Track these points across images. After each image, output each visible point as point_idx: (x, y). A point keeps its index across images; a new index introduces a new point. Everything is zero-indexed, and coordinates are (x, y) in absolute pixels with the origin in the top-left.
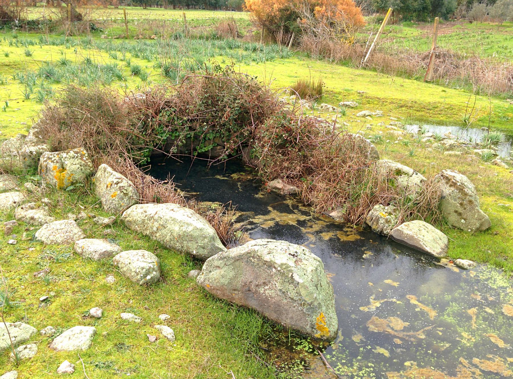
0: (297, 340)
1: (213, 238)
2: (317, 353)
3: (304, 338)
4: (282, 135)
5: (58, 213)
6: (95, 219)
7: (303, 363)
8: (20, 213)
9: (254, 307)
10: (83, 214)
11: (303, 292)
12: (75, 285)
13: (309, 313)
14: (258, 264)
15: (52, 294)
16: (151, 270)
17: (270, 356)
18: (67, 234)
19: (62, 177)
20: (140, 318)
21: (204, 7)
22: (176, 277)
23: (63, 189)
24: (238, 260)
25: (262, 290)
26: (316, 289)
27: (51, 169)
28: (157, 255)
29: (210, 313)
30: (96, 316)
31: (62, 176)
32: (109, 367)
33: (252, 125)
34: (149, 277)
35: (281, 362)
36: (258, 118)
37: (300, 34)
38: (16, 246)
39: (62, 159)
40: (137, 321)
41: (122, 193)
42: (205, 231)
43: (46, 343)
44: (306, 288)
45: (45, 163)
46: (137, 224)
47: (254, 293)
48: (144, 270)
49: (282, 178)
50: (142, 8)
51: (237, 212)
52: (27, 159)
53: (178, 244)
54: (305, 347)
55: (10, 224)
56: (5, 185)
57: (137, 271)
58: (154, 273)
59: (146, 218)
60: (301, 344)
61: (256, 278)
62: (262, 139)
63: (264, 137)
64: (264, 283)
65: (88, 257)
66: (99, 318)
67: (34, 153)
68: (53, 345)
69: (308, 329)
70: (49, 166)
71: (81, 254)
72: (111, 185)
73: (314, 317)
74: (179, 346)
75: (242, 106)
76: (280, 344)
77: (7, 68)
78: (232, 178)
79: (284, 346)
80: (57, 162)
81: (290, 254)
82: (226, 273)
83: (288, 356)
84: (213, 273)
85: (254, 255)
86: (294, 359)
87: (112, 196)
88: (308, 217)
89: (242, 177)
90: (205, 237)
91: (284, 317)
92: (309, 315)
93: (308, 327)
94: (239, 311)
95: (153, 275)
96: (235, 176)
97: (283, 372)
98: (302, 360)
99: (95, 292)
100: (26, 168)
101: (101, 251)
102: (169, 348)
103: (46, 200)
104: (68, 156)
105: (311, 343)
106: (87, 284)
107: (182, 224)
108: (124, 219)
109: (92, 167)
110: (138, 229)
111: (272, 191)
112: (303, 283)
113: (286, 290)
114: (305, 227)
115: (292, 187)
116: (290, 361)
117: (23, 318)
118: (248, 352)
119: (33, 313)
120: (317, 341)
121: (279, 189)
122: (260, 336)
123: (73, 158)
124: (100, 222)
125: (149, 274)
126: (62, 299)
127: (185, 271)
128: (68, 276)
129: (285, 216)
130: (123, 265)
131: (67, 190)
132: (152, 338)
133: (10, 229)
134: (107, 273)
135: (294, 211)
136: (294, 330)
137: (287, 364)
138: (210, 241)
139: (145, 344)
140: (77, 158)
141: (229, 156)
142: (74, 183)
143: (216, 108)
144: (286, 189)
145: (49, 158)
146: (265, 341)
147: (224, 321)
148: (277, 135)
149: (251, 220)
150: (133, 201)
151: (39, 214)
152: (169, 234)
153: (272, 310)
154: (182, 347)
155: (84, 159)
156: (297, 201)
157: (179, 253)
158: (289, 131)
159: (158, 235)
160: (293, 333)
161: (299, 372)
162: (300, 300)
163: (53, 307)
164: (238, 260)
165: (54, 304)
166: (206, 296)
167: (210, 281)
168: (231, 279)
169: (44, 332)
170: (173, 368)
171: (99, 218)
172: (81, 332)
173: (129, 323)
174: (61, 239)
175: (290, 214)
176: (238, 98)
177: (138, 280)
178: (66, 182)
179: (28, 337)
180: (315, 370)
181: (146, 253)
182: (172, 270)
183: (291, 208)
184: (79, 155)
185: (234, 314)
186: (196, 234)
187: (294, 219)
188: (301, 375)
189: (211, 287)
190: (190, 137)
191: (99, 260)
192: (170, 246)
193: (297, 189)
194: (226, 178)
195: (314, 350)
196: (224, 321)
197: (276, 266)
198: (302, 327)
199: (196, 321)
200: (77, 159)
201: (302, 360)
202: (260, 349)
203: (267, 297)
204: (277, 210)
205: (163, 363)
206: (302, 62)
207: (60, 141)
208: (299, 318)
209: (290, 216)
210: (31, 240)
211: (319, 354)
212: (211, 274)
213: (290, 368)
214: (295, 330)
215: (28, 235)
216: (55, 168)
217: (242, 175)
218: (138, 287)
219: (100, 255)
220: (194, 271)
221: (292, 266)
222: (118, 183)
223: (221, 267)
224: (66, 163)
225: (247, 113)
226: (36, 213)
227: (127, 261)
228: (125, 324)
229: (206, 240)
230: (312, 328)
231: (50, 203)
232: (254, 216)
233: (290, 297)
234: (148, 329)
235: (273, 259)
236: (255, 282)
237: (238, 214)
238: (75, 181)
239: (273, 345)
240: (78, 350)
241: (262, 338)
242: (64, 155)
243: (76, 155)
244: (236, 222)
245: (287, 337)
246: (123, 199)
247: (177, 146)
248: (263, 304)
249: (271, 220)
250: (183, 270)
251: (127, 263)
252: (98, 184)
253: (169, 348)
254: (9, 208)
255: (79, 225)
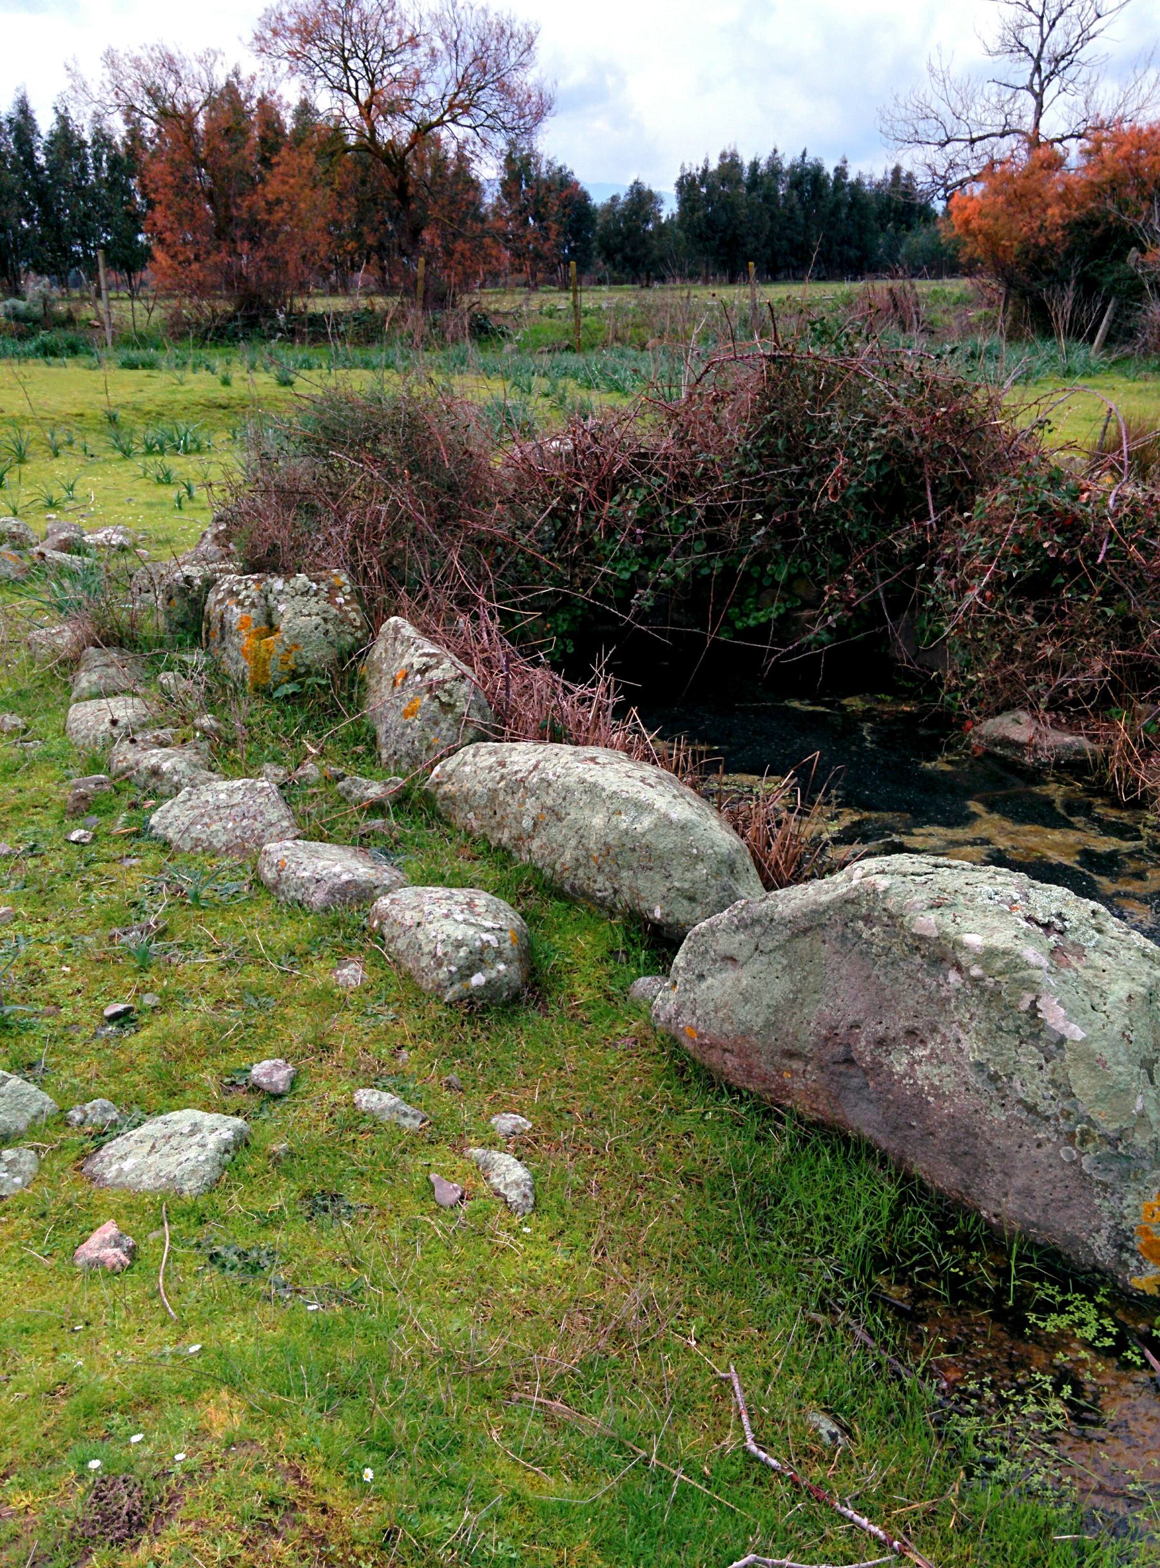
0: (1047, 1291)
1: (731, 866)
2: (1138, 1361)
3: (1078, 1288)
4: (1039, 545)
5: (234, 762)
6: (341, 784)
7: (1067, 1390)
8: (125, 755)
9: (867, 1132)
10: (310, 769)
11: (1082, 1082)
12: (228, 981)
13: (1108, 1178)
14: (887, 951)
15: (149, 1000)
16: (489, 956)
17: (919, 1339)
18: (245, 822)
19: (263, 654)
20: (425, 1114)
21: (824, 273)
22: (584, 995)
23: (264, 692)
24: (806, 931)
25: (899, 1063)
26: (1144, 1076)
27: (235, 628)
28: (524, 915)
29: (688, 1135)
30: (266, 1087)
31: (263, 648)
32: (256, 1268)
33: (927, 516)
34: (478, 979)
35: (964, 1371)
36: (951, 498)
37: (1139, 301)
38: (87, 849)
39: (271, 597)
40: (406, 1122)
41: (436, 703)
42: (699, 831)
43: (74, 1156)
44: (1097, 1064)
45: (218, 609)
46: (472, 808)
47: (866, 1072)
48: (463, 952)
49: (1032, 708)
50: (638, 286)
51: (846, 810)
52: (176, 601)
53: (600, 879)
54: (1082, 1323)
55: (87, 784)
56: (107, 677)
57: (440, 954)
58: (502, 967)
59: (503, 784)
60: (1061, 1309)
61: (879, 1008)
62: (963, 563)
63: (968, 555)
64: (911, 1033)
65: (293, 899)
66: (277, 1097)
67: (198, 582)
68: (94, 1166)
69: (1101, 1248)
70: (227, 616)
71: (275, 887)
72: (406, 677)
73: (1130, 1199)
74: (542, 1237)
75: (894, 452)
76: (967, 1296)
77: (220, 413)
78: (843, 707)
79: (984, 1307)
80: (253, 605)
81: (1029, 919)
82: (758, 985)
83: (998, 1348)
84: (710, 981)
85: (873, 909)
86: (1026, 1366)
87: (406, 714)
88: (1131, 844)
89: (880, 707)
90: (699, 858)
91: (991, 1186)
92: (1106, 1186)
93: (1100, 1240)
94: (805, 1141)
95: (494, 974)
96: (855, 703)
97: (967, 1414)
98: (1063, 1376)
99: (289, 1012)
100: (173, 633)
101: (336, 880)
102: (504, 1239)
103: (207, 721)
104: (287, 589)
105: (1111, 1313)
106: (269, 979)
107: (619, 803)
108: (433, 790)
109: (361, 628)
110: (475, 824)
111: (989, 755)
112: (1084, 1041)
113: (1005, 1065)
114: (1114, 877)
115: (1068, 739)
116: (1007, 1372)
117: (31, 1066)
118: (823, 1307)
119: (69, 1054)
120: (1139, 1309)
121: (1018, 746)
122: (884, 1248)
123: (302, 594)
124: (356, 793)
125: (479, 970)
126: (175, 1020)
127: (619, 981)
128: (214, 952)
129: (1035, 833)
130: (397, 930)
131: (276, 695)
132: (448, 1192)
133: (83, 798)
134: (342, 956)
135: (1072, 819)
136: (1034, 1246)
137: (993, 1386)
138: (718, 874)
139: (413, 1209)
140: (316, 595)
141: (840, 631)
142: (301, 676)
143: (798, 464)
144: (1045, 745)
145: (232, 593)
146: (904, 1271)
147: (741, 1171)
148: (1022, 546)
149: (896, 838)
150: (471, 733)
151: (170, 761)
152: (573, 843)
153: (942, 1152)
154: (554, 1243)
155: (340, 600)
156: (1085, 790)
157: (605, 914)
158: (1071, 526)
159: (535, 844)
160: (1030, 1260)
161: (1045, 1428)
162: (1067, 1115)
163: (136, 1041)
164: (806, 931)
165: (146, 1033)
166: (681, 1071)
167: (699, 1012)
168: (777, 1009)
169: (78, 1117)
170: (503, 1315)
171: (354, 782)
172: (195, 1129)
173: (377, 1127)
174: (224, 838)
175: (1054, 828)
176: (881, 422)
177: (439, 986)
178: (274, 669)
179: (22, 1127)
180: (1122, 1432)
181: (482, 899)
182: (571, 969)
183: (1062, 811)
184: (322, 586)
185: (784, 1148)
186: (665, 843)
187: (1072, 846)
188: (1053, 1442)
189: (701, 1036)
190: (711, 575)
191: (326, 910)
192: (573, 887)
193: (1088, 746)
194: (822, 709)
195: (1122, 1344)
196: (741, 1171)
197: (963, 958)
198: (1072, 1240)
199: (631, 1154)
200: (315, 599)
201: (1063, 1376)
202: (876, 1300)
203: (918, 1094)
204: (1005, 814)
205: (466, 1290)
206: (1140, 385)
207: (275, 545)
208: (1060, 1194)
209: (1056, 836)
210: (137, 835)
211: (1146, 1365)
212: (704, 986)
213: (1003, 1402)
214: (1039, 1247)
215: (129, 822)
216: (244, 624)
217: (880, 701)
218: (436, 1011)
219: (331, 893)
220: (648, 979)
221: (1033, 960)
222: (426, 670)
223: (741, 959)
224: (281, 608)
225: (912, 476)
226: (169, 757)
227: (409, 918)
228: (362, 1127)
229: (702, 870)
230: (1121, 1247)
231: (217, 731)
232: (909, 827)
233: (1020, 1101)
234: (441, 1157)
235: (951, 929)
236: (873, 1028)
237: (849, 817)
238: (302, 670)
239: (937, 1296)
240: (165, 1195)
241: (891, 1261)
242: (278, 584)
243: (314, 585)
244: (836, 841)
245: (1003, 1273)
246: (436, 723)
247: (655, 586)
248: (901, 1121)
249: (973, 843)
250: (611, 977)
251: (408, 923)
252: (373, 682)
253: (504, 1239)
254: (100, 741)
255: (288, 801)
